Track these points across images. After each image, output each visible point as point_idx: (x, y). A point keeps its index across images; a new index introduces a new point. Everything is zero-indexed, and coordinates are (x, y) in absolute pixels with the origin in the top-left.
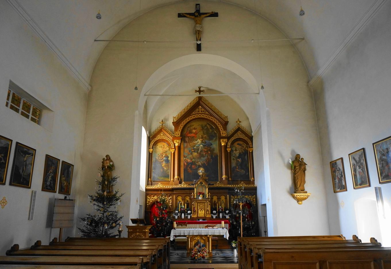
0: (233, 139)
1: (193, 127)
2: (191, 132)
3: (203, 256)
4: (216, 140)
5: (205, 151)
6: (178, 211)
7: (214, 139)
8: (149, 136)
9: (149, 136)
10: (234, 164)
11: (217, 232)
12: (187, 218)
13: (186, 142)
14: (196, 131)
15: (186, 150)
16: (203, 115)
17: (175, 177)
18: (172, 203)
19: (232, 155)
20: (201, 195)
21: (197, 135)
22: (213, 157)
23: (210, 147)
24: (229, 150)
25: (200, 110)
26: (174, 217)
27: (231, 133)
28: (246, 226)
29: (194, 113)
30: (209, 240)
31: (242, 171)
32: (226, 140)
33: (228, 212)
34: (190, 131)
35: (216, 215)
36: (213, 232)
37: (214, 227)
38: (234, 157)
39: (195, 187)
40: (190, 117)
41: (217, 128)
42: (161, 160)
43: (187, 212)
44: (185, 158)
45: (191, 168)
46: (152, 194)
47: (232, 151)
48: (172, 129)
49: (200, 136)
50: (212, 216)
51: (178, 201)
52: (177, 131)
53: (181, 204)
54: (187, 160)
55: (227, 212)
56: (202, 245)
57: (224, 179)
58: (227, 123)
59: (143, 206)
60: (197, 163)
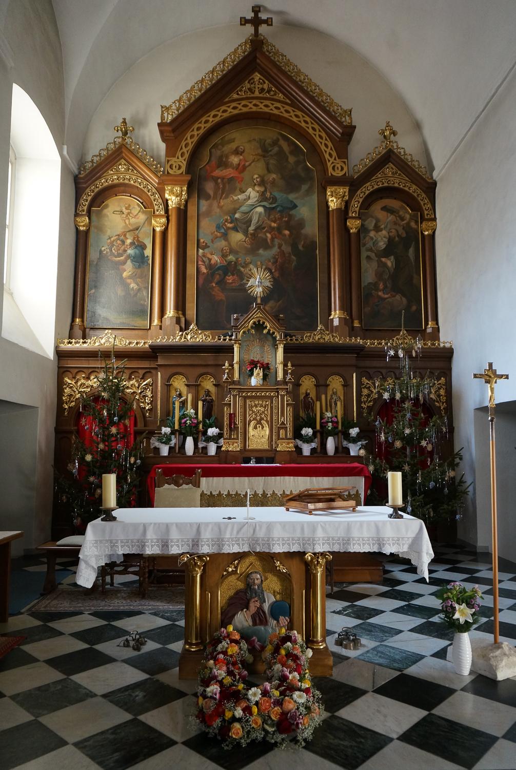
0: (368, 188)
1: (233, 146)
2: (223, 163)
3: (284, 714)
4: (309, 192)
5: (273, 228)
6: (172, 427)
7: (305, 187)
8: (76, 172)
9: (76, 172)
10: (369, 274)
11: (366, 534)
12: (206, 454)
13: (208, 197)
14: (240, 160)
15: (205, 223)
16: (268, 103)
17: (168, 313)
18: (151, 403)
19: (364, 245)
20: (256, 372)
21: (246, 175)
22: (300, 247)
23: (291, 217)
24: (353, 225)
25: (258, 86)
26: (157, 450)
27: (362, 169)
28: (432, 484)
29: (235, 96)
30: (315, 576)
31: (398, 297)
32: (343, 190)
33: (358, 434)
34: (221, 157)
35: (314, 445)
36: (341, 533)
37: (336, 504)
38: (371, 250)
39: (236, 340)
40: (223, 108)
41: (314, 148)
42: (120, 255)
43: (205, 433)
44: (201, 251)
45: (222, 282)
46: (80, 370)
47: (363, 230)
48: (159, 157)
49: (256, 176)
50: (297, 447)
51: (174, 394)
52: (174, 156)
53: (183, 404)
54: (210, 256)
55: (354, 432)
56: (273, 606)
57: (336, 322)
58: (349, 132)
59: (41, 414)
60: (242, 269)
